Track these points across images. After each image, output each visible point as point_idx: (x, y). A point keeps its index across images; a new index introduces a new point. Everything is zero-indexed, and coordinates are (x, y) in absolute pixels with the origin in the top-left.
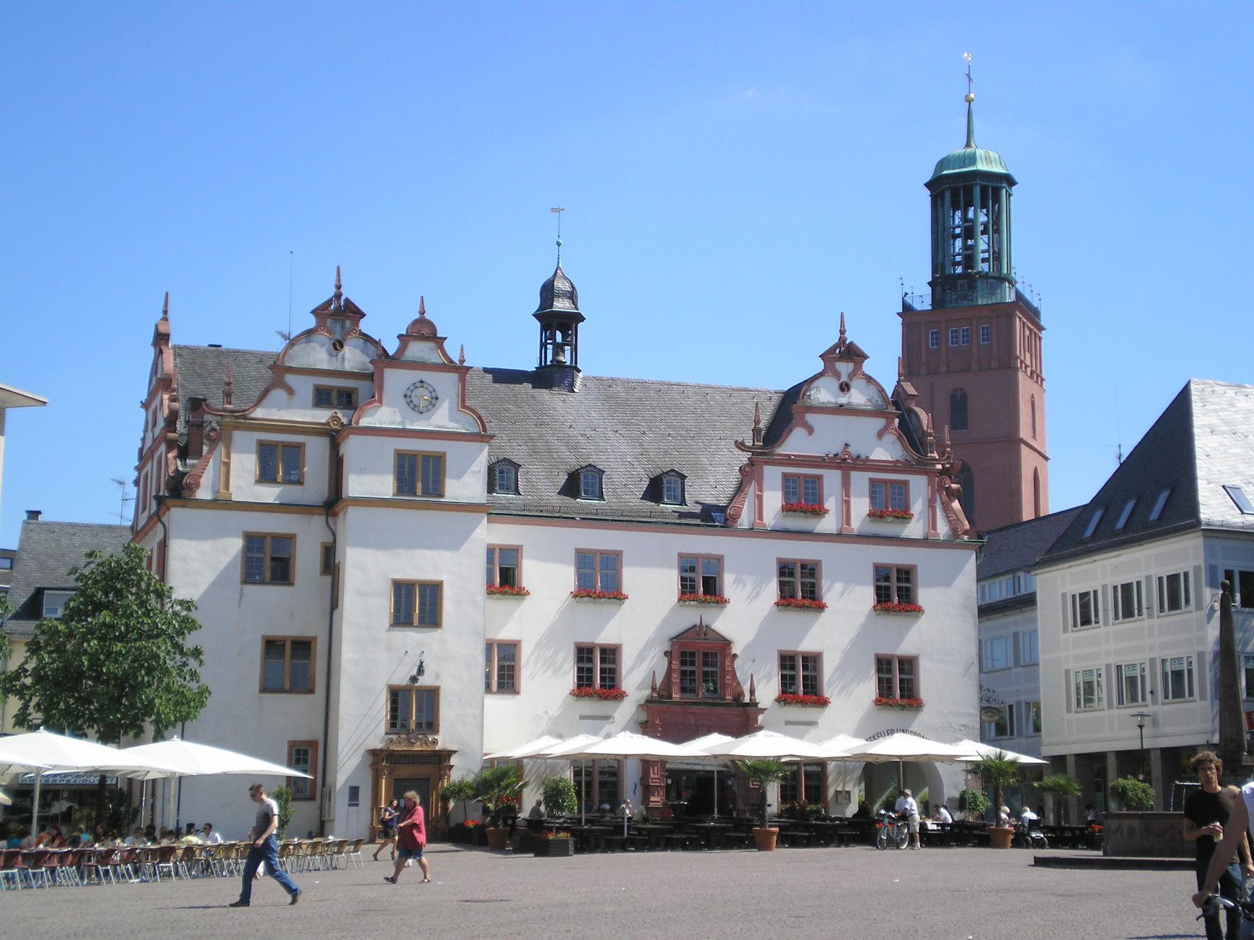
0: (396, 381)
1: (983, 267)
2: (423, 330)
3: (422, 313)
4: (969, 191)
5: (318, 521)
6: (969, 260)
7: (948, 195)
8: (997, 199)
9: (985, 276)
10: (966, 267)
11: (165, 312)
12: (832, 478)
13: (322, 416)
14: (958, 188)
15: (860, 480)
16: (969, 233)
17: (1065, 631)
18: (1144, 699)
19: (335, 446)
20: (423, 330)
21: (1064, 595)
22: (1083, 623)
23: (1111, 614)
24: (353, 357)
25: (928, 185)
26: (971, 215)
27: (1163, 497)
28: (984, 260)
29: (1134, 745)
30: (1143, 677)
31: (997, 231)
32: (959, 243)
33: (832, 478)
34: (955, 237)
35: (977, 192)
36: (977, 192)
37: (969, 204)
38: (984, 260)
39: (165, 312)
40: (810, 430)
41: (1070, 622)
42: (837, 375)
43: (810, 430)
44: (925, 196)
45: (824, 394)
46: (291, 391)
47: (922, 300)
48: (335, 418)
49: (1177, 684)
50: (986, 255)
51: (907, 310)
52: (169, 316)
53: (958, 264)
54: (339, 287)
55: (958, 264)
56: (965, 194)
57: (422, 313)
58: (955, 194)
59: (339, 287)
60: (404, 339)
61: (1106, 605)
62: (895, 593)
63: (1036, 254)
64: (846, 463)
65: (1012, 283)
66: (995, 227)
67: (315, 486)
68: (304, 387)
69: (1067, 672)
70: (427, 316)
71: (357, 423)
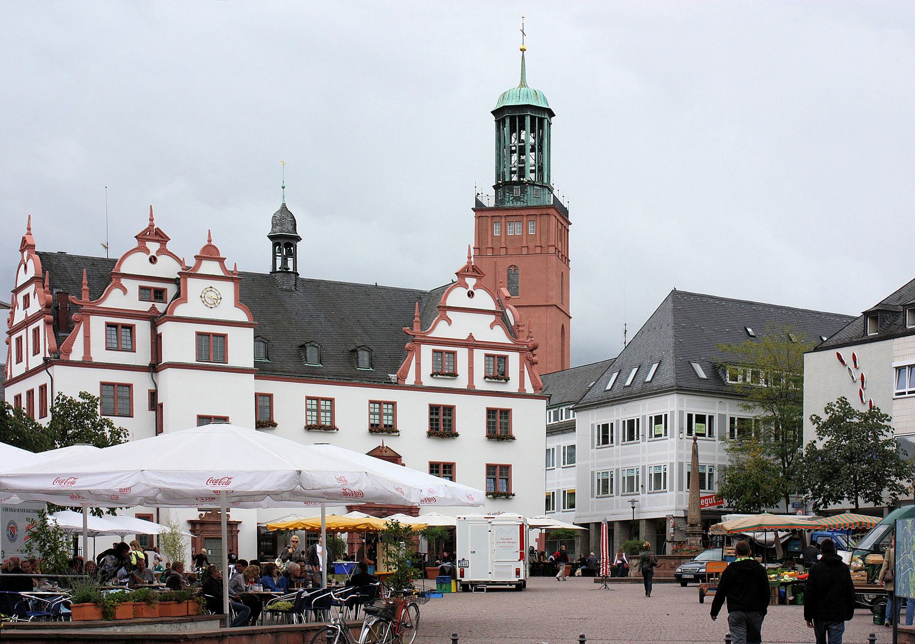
0: (194, 286)
1: (532, 176)
2: (210, 253)
3: (210, 241)
4: (522, 119)
5: (145, 376)
6: (521, 172)
7: (508, 121)
8: (541, 126)
9: (533, 184)
10: (519, 177)
11: (29, 229)
12: (462, 354)
13: (145, 306)
14: (515, 117)
15: (479, 354)
16: (522, 151)
17: (593, 447)
18: (637, 490)
19: (154, 328)
20: (210, 253)
21: (593, 425)
22: (603, 444)
23: (621, 439)
24: (167, 268)
25: (494, 113)
26: (523, 137)
27: (655, 366)
28: (532, 171)
29: (629, 517)
30: (638, 477)
31: (541, 150)
32: (515, 157)
33: (462, 354)
34: (513, 152)
35: (528, 120)
36: (528, 120)
37: (522, 127)
38: (532, 171)
39: (29, 229)
40: (449, 322)
41: (596, 442)
42: (466, 286)
43: (449, 322)
44: (491, 122)
45: (457, 298)
46: (125, 291)
47: (490, 201)
48: (153, 308)
49: (659, 480)
50: (533, 168)
51: (479, 208)
52: (32, 231)
53: (514, 172)
54: (152, 220)
55: (514, 172)
56: (523, 122)
57: (210, 241)
58: (513, 120)
59: (152, 220)
60: (199, 259)
61: (618, 433)
62: (499, 427)
63: (570, 171)
64: (471, 344)
65: (551, 190)
66: (540, 147)
67: (142, 356)
68: (133, 286)
69: (593, 473)
70: (213, 243)
71: (172, 312)
